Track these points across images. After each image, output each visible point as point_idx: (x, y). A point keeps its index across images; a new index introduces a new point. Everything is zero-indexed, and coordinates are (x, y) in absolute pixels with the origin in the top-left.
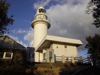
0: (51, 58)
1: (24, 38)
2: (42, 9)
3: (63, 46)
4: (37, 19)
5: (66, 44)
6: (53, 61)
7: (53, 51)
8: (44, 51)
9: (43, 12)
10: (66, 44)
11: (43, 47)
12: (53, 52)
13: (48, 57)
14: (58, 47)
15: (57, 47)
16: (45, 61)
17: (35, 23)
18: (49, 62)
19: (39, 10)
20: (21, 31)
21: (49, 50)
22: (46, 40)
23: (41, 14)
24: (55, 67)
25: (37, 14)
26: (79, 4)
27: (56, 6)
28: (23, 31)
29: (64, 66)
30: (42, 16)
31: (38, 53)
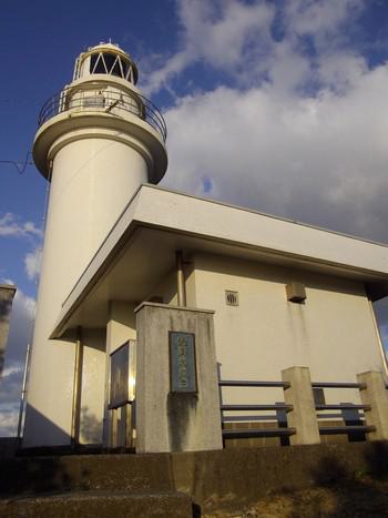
0: (181, 402)
1: (24, 265)
2: (110, 57)
3: (278, 291)
4: (78, 109)
5: (299, 274)
6: (202, 435)
7: (209, 324)
8: (118, 333)
9: (117, 72)
10: (299, 274)
11: (110, 302)
12: (201, 342)
13: (146, 384)
14: (241, 299)
15: (232, 299)
16: (124, 414)
17: (57, 143)
18: (164, 446)
19: (94, 58)
20: (9, 224)
21: (158, 321)
22: (137, 228)
23: (105, 84)
24: (231, 496)
25: (74, 83)
26: (326, 93)
27: (211, 96)
28: (23, 228)
29: (320, 483)
30: (112, 94)
31: (69, 349)
